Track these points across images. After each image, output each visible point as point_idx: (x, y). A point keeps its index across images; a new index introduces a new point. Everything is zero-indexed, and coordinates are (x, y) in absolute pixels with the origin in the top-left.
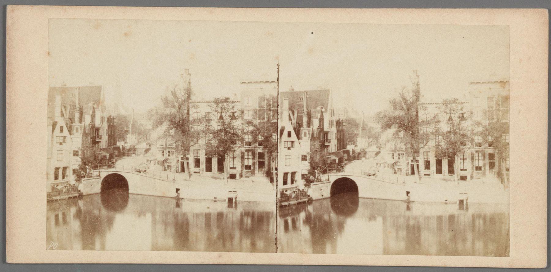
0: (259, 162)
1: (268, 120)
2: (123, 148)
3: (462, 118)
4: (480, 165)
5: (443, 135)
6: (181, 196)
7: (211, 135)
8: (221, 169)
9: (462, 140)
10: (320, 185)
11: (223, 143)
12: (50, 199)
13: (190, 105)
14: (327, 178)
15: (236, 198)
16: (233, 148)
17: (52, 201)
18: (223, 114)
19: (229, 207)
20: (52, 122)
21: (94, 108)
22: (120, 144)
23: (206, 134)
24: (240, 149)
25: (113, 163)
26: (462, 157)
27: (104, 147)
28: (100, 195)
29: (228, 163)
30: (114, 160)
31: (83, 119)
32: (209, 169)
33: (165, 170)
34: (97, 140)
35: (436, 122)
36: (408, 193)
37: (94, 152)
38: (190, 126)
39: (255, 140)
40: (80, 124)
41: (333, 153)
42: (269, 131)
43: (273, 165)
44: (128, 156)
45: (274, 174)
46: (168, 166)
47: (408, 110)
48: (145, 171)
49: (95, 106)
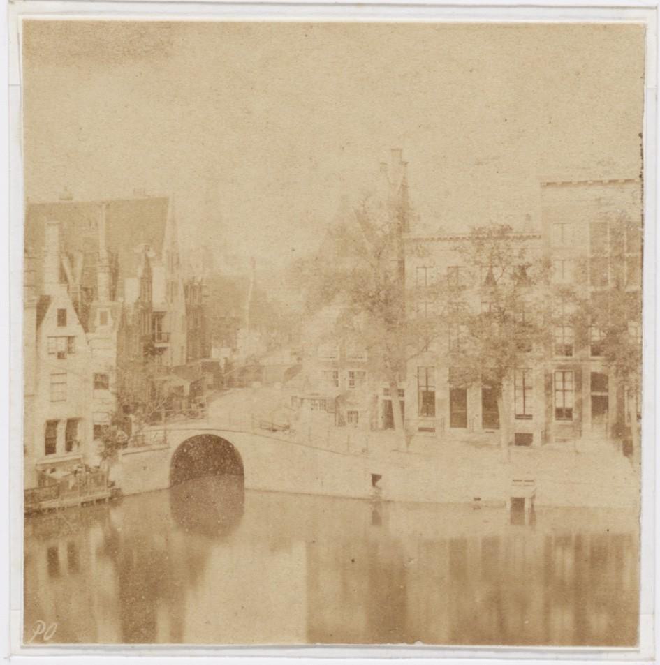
0: (594, 398)
1: (618, 287)
2: (229, 366)
3: (521, 275)
4: (569, 405)
5: (471, 322)
6: (384, 495)
7: (463, 328)
8: (491, 418)
9: (519, 336)
10: (144, 455)
11: (496, 347)
12: (35, 507)
13: (406, 247)
14: (161, 435)
15: (533, 498)
16: (522, 362)
17: (39, 513)
18: (495, 271)
19: (512, 521)
20: (36, 298)
21: (147, 260)
22: (219, 354)
23: (450, 325)
24: (540, 366)
25: (202, 405)
26: (519, 383)
27: (177, 363)
28: (166, 496)
29: (509, 403)
30: (203, 399)
31: (119, 290)
32: (460, 419)
33: (341, 423)
34: (157, 346)
35: (451, 289)
36: (375, 478)
37: (151, 377)
38: (408, 303)
39: (583, 340)
40: (110, 303)
41: (177, 370)
42: (621, 314)
43: (630, 406)
44: (241, 386)
45: (634, 430)
46: (350, 413)
47: (378, 255)
48: (287, 427)
49: (151, 254)
